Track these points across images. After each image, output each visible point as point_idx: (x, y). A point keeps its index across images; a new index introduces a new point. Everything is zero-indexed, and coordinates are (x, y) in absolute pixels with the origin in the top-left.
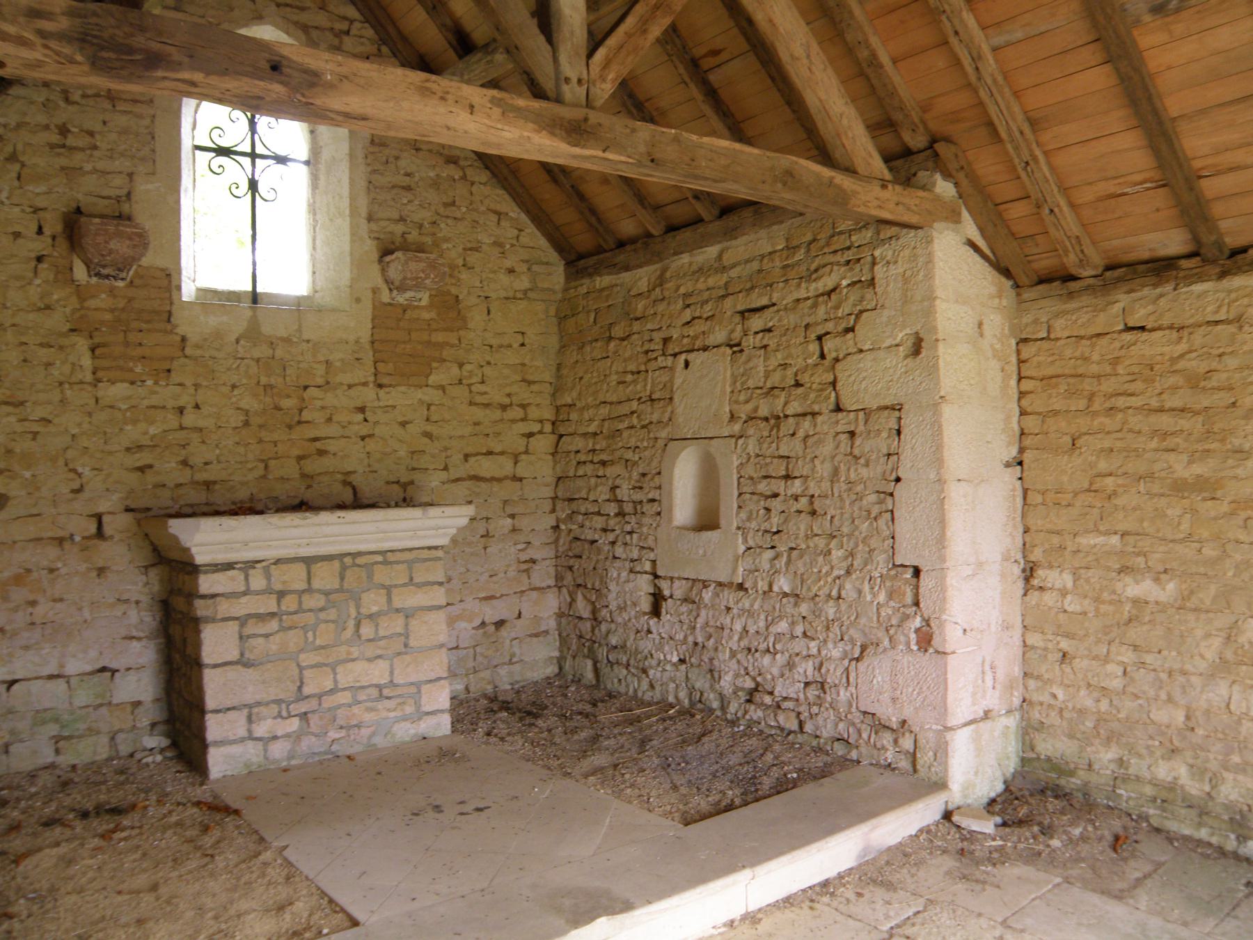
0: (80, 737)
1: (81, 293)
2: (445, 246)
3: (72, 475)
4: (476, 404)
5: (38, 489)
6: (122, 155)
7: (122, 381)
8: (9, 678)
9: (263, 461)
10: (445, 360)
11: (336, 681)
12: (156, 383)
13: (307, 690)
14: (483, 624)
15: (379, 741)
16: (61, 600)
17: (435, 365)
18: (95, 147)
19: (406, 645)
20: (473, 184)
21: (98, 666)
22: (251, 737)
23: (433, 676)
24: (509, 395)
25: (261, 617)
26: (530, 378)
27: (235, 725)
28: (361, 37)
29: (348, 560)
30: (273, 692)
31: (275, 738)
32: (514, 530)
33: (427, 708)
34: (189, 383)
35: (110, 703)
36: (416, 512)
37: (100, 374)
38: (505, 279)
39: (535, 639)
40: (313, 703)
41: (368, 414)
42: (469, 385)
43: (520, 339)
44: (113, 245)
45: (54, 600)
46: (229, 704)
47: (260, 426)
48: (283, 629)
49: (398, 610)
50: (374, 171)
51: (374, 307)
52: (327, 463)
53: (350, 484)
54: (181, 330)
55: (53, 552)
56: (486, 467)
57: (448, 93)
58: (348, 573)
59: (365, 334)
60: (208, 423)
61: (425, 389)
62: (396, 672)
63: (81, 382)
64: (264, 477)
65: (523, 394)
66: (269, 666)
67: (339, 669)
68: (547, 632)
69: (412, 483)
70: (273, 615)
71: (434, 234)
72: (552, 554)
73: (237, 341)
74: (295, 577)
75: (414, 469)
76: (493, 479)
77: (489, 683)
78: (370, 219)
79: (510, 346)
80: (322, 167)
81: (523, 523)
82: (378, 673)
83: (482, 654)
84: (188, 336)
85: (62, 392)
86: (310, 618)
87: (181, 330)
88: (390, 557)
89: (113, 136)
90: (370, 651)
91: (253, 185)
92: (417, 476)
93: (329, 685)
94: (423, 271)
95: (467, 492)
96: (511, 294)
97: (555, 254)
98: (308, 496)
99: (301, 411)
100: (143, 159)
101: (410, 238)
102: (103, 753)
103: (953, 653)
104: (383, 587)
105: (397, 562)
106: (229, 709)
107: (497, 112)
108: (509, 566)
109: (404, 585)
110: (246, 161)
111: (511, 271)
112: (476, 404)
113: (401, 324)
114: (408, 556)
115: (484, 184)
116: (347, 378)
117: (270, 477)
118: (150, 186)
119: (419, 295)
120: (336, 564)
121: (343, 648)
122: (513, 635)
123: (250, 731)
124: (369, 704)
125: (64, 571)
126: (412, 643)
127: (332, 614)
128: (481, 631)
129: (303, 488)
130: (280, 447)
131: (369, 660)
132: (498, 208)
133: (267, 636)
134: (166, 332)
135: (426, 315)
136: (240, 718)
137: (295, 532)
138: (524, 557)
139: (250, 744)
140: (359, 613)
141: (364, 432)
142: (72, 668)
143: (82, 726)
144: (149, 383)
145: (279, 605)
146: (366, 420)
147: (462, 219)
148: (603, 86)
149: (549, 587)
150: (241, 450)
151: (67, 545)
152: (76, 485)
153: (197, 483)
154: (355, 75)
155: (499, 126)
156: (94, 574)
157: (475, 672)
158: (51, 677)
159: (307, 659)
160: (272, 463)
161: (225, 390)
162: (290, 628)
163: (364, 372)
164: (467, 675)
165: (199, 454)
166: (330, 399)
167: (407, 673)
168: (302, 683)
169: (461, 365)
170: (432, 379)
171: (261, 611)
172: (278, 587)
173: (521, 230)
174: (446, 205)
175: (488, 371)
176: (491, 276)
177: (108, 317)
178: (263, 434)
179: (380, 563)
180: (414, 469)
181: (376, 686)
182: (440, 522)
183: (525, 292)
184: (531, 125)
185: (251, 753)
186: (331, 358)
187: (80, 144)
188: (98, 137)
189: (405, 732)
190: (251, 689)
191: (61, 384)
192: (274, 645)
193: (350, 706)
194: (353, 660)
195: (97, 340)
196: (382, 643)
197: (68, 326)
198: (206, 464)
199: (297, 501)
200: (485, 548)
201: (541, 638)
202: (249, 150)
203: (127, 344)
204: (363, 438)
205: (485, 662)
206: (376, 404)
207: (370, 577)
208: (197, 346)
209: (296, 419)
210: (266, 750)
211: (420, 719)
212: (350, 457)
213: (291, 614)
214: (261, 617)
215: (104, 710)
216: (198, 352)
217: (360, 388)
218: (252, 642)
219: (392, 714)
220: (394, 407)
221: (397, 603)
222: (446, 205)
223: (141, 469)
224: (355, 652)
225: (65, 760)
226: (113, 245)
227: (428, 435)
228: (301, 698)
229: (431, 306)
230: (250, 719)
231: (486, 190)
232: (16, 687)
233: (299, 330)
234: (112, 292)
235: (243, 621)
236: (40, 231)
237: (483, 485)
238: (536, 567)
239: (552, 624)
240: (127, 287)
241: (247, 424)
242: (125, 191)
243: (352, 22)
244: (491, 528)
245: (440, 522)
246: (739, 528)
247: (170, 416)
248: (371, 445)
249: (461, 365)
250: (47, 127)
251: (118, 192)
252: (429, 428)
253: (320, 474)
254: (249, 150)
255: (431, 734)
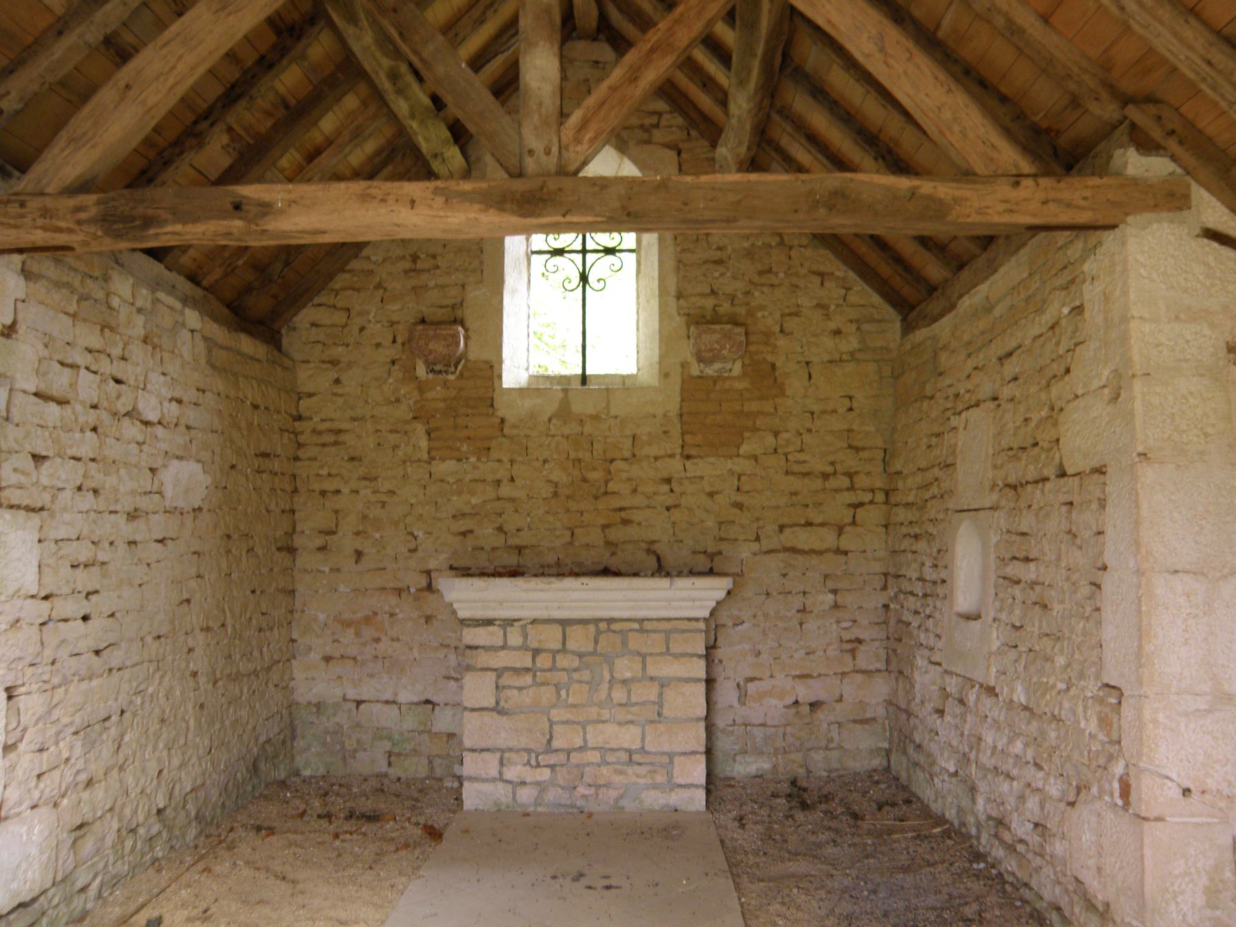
0: (406, 755)
1: (422, 388)
2: (759, 314)
3: (410, 537)
4: (793, 473)
5: (384, 547)
6: (457, 270)
7: (451, 459)
8: (358, 698)
9: (570, 529)
10: (759, 430)
11: (585, 740)
12: (479, 459)
13: (556, 744)
14: (797, 702)
15: (628, 805)
16: (398, 640)
17: (746, 434)
18: (437, 267)
19: (659, 714)
20: (791, 248)
21: (423, 698)
22: (501, 778)
23: (689, 748)
24: (832, 463)
25: (517, 671)
26: (859, 444)
27: (488, 765)
28: (671, 127)
29: (603, 626)
30: (524, 741)
31: (523, 783)
32: (836, 606)
33: (680, 781)
34: (506, 459)
35: (430, 732)
36: (664, 582)
37: (433, 454)
38: (829, 342)
39: (858, 726)
40: (562, 757)
41: (674, 485)
42: (786, 454)
43: (847, 403)
44: (432, 346)
45: (393, 640)
46: (483, 745)
47: (568, 497)
48: (536, 684)
49: (652, 679)
50: (684, 250)
51: (683, 381)
52: (632, 532)
53: (654, 552)
54: (500, 413)
55: (393, 600)
56: (803, 538)
57: (388, 194)
58: (602, 638)
59: (674, 406)
60: (521, 494)
61: (736, 460)
62: (647, 740)
63: (419, 460)
64: (571, 543)
65: (850, 461)
66: (522, 716)
67: (589, 728)
68: (874, 719)
69: (720, 553)
70: (528, 670)
71: (748, 304)
72: (883, 635)
73: (550, 420)
74: (550, 637)
75: (721, 539)
76: (812, 551)
77: (801, 766)
78: (679, 296)
79: (835, 411)
80: (643, 253)
81: (847, 599)
82: (629, 737)
83: (793, 736)
84: (507, 417)
85: (405, 469)
86: (563, 677)
87: (500, 413)
88: (647, 626)
89: (452, 255)
90: (622, 715)
91: (584, 278)
92: (724, 547)
93: (578, 742)
94: (717, 342)
95: (781, 565)
96: (837, 357)
97: (891, 310)
98: (613, 563)
99: (607, 482)
100: (474, 271)
101: (721, 310)
102: (423, 772)
103: (1159, 819)
104: (639, 654)
105: (654, 631)
106: (483, 750)
107: (440, 200)
108: (828, 645)
109: (661, 654)
110: (590, 258)
111: (837, 332)
112: (793, 473)
113: (712, 396)
114: (667, 626)
115: (805, 247)
116: (653, 451)
117: (577, 544)
118: (477, 293)
119: (729, 366)
120: (592, 628)
121: (594, 710)
122: (832, 718)
123: (501, 773)
124: (619, 767)
125: (400, 616)
126: (665, 712)
127: (586, 675)
128: (793, 711)
129: (608, 554)
130: (586, 517)
131: (620, 724)
132: (822, 268)
133: (520, 689)
134: (488, 415)
135: (740, 385)
136: (492, 760)
137: (542, 595)
138: (847, 636)
139: (500, 785)
140: (612, 677)
141: (670, 502)
142: (405, 697)
143: (408, 747)
144: (473, 460)
145: (534, 661)
146: (672, 491)
147: (781, 285)
148: (579, 148)
149: (879, 671)
150: (550, 518)
151: (404, 595)
152: (412, 545)
153: (510, 547)
154: (302, 198)
155: (442, 214)
156: (423, 621)
157: (785, 752)
158: (387, 702)
159: (556, 714)
160: (578, 531)
161: (537, 464)
162: (543, 684)
163: (673, 444)
164: (775, 755)
165: (512, 521)
166: (635, 471)
167: (659, 741)
168: (551, 737)
169: (776, 434)
170: (744, 449)
171: (518, 666)
172: (535, 645)
173: (848, 289)
174: (761, 273)
175: (807, 438)
176: (813, 340)
177: (441, 405)
178: (571, 504)
179: (637, 631)
180: (721, 539)
181: (627, 750)
182: (694, 594)
183: (852, 354)
184: (477, 206)
185: (501, 792)
186: (638, 432)
187: (426, 266)
188: (439, 258)
189: (655, 800)
190: (503, 735)
191: (404, 462)
192: (527, 698)
193: (599, 765)
194: (603, 722)
195: (432, 425)
196: (634, 709)
197: (411, 415)
198: (518, 530)
199: (601, 567)
200: (801, 624)
201: (867, 726)
202: (580, 248)
203: (456, 427)
204: (668, 509)
205: (798, 744)
206: (683, 474)
207: (624, 643)
208: (514, 427)
209: (602, 490)
210: (514, 794)
211: (671, 790)
212: (656, 527)
213: (544, 670)
214: (517, 671)
215: (425, 736)
216: (516, 432)
217: (667, 460)
218: (508, 692)
219: (641, 781)
220: (702, 478)
221: (652, 671)
222: (761, 273)
223: (464, 534)
224: (606, 714)
225: (394, 772)
226: (432, 346)
227: (739, 506)
228: (549, 750)
229: (745, 374)
230: (502, 764)
231: (808, 252)
232: (362, 706)
233: (608, 407)
234: (445, 384)
235: (500, 672)
236: (394, 341)
237: (800, 558)
238: (862, 648)
239: (881, 711)
240: (458, 378)
241: (555, 494)
242: (459, 300)
243: (660, 114)
244: (809, 603)
245: (694, 594)
246: (995, 620)
247: (489, 488)
248: (676, 515)
249: (776, 434)
250: (403, 258)
251: (453, 301)
252: (740, 498)
253: (624, 542)
254: (588, 247)
255: (683, 807)
